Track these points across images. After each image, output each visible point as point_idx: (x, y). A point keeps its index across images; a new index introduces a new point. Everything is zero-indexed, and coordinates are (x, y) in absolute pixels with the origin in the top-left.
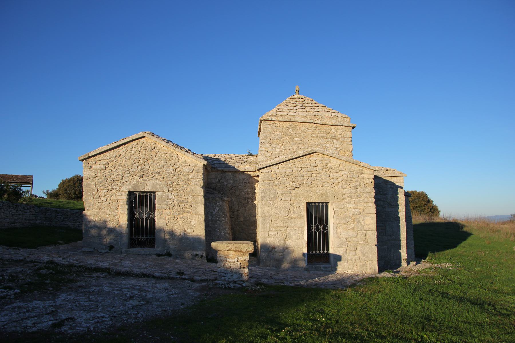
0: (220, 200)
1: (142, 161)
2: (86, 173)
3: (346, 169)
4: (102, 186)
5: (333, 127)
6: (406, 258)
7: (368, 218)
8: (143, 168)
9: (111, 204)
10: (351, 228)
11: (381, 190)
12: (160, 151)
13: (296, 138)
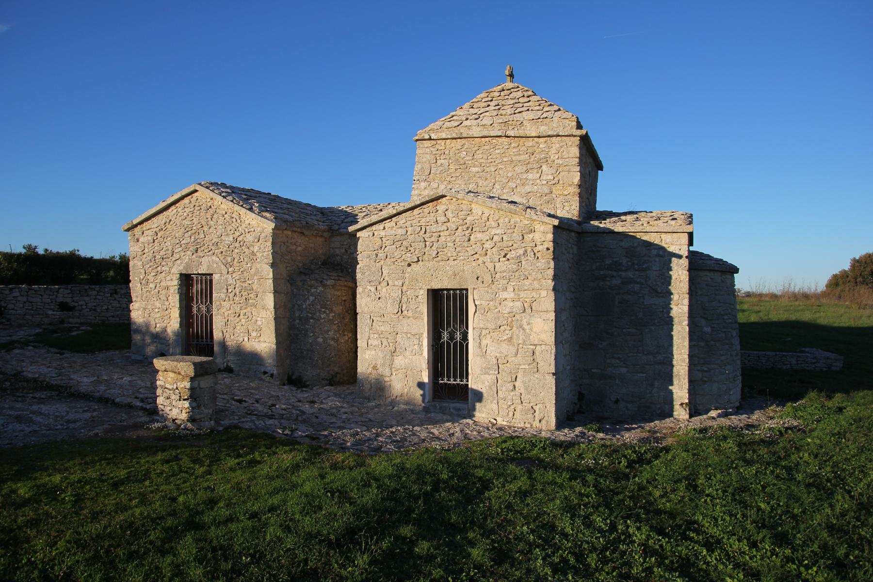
0: (320, 284)
1: (195, 228)
2: (132, 249)
3: (501, 225)
4: (150, 267)
5: (541, 140)
6: (687, 401)
7: (539, 320)
8: (196, 238)
9: (160, 292)
10: (505, 338)
11: (636, 262)
12: (218, 211)
13: (474, 167)
